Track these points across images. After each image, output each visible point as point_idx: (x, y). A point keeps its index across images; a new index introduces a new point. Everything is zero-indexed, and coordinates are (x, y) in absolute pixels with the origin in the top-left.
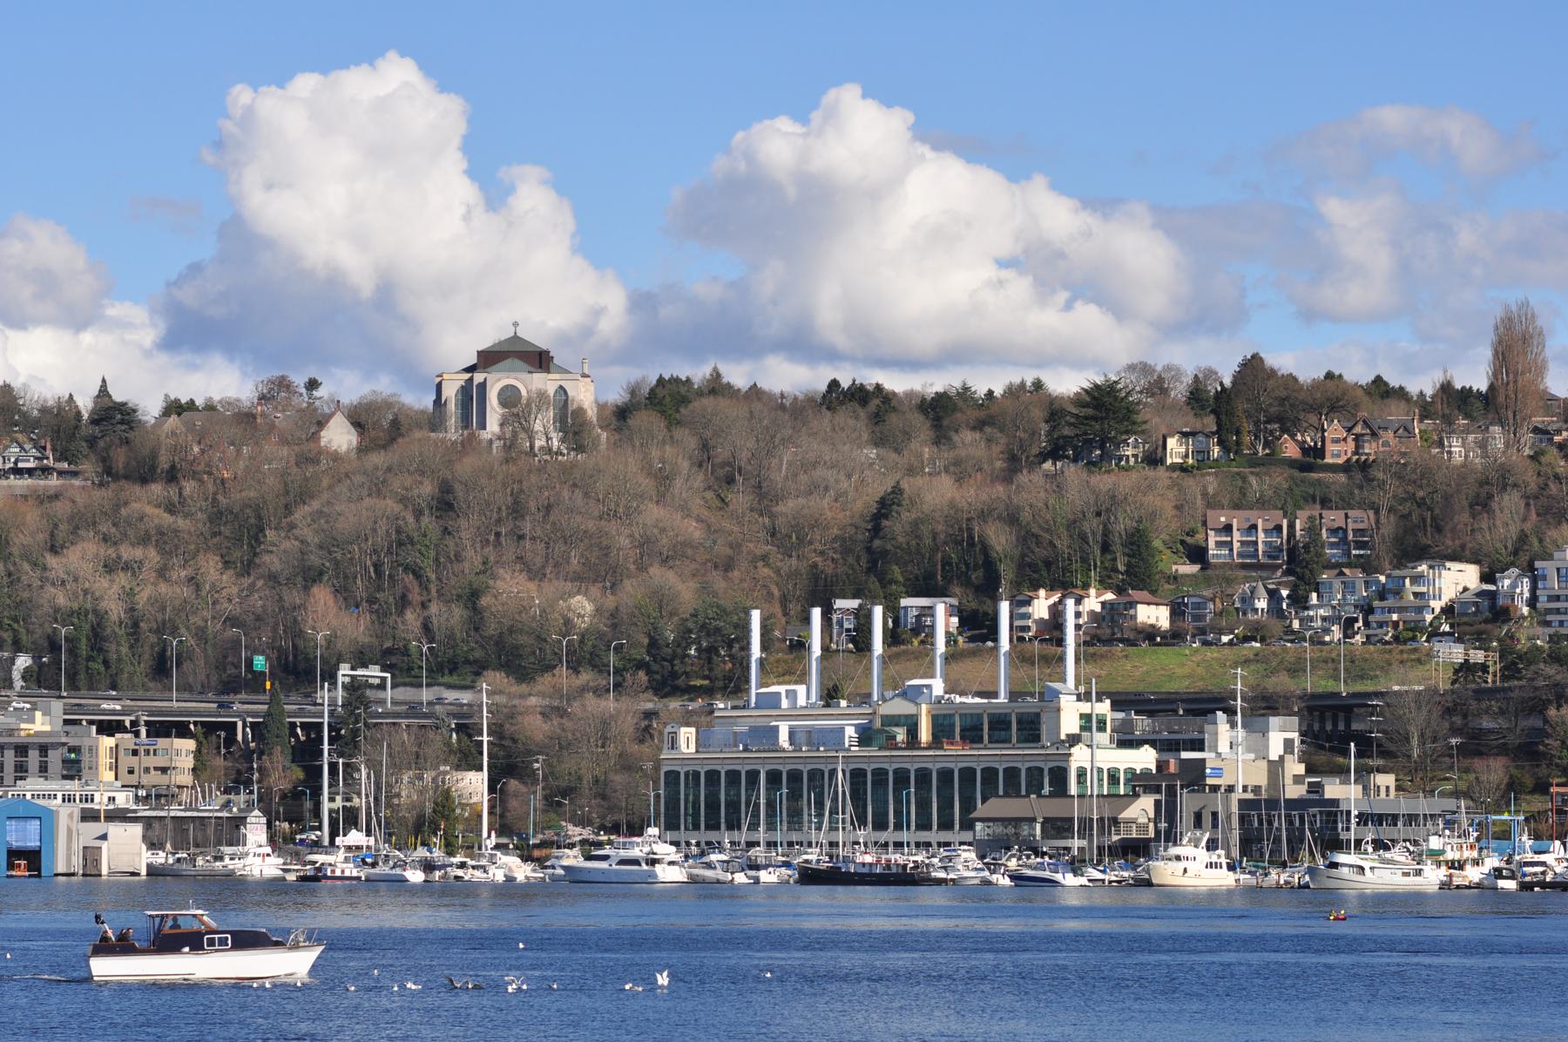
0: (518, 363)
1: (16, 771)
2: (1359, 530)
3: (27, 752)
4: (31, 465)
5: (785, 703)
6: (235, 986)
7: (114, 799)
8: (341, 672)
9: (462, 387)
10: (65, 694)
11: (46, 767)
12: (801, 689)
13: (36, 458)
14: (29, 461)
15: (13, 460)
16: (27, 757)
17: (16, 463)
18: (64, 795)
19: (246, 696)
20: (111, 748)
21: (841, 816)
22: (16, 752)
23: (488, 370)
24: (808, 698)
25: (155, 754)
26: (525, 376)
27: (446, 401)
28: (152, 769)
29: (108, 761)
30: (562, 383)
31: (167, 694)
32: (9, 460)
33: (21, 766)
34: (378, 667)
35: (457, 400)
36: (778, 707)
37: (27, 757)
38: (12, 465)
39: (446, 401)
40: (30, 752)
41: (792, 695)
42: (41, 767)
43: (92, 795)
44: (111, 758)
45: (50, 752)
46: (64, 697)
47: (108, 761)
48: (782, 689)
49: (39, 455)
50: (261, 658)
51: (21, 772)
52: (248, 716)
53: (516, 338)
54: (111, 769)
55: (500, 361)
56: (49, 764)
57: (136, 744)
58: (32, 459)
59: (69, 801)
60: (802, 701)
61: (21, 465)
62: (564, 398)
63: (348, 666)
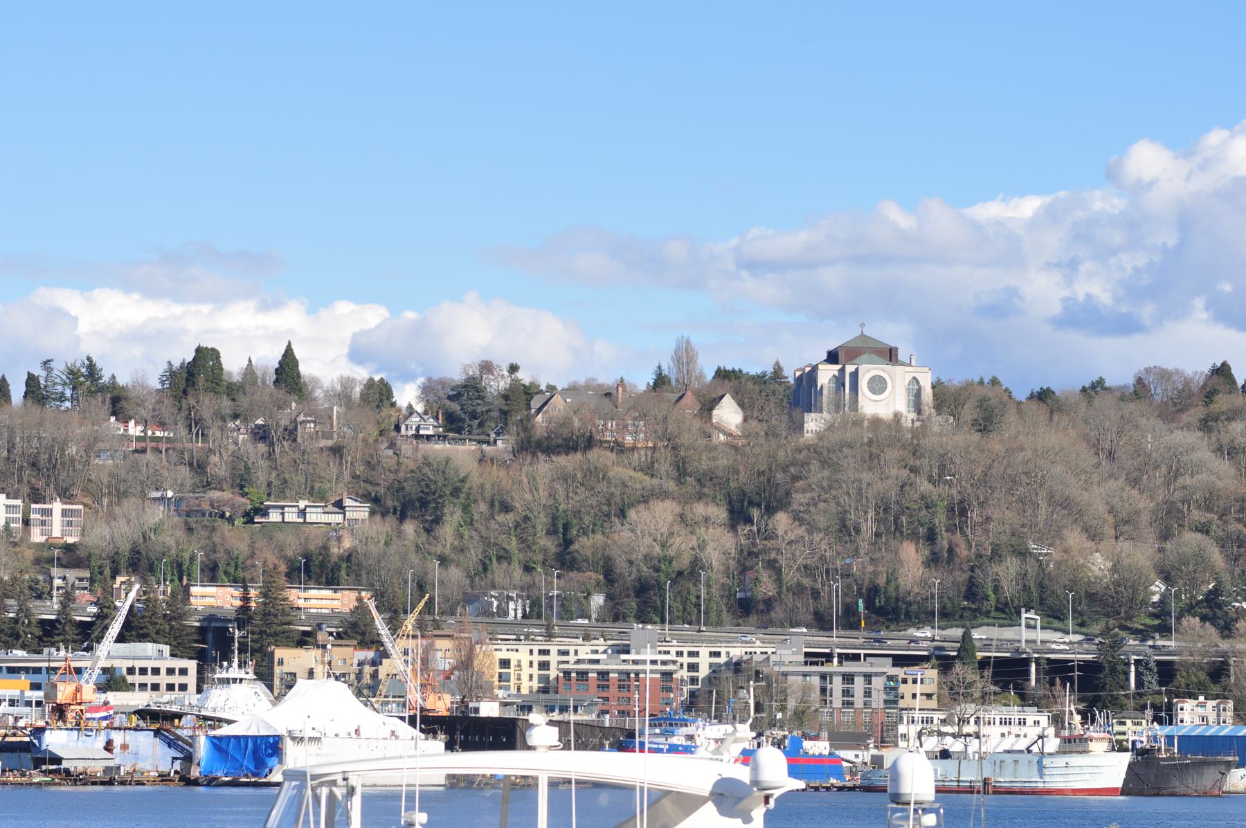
0: (874, 357)
1: (843, 696)
2: (10, 506)
3: (853, 680)
4: (430, 432)
7: (1038, 722)
9: (834, 376)
10: (704, 629)
11: (870, 692)
13: (434, 427)
14: (428, 429)
15: (414, 428)
16: (853, 684)
17: (418, 429)
18: (1001, 719)
19: (842, 633)
21: (637, 740)
22: (843, 679)
25: (922, 683)
27: (822, 387)
28: (137, 686)
30: (916, 375)
31: (829, 633)
32: (411, 428)
33: (848, 691)
37: (853, 684)
38: (414, 432)
39: (822, 387)
42: (865, 692)
43: (1024, 719)
45: (873, 679)
46: (703, 631)
51: (848, 696)
52: (1134, 654)
53: (863, 337)
57: (905, 674)
58: (431, 427)
59: (1005, 723)
61: (422, 432)
62: (916, 387)
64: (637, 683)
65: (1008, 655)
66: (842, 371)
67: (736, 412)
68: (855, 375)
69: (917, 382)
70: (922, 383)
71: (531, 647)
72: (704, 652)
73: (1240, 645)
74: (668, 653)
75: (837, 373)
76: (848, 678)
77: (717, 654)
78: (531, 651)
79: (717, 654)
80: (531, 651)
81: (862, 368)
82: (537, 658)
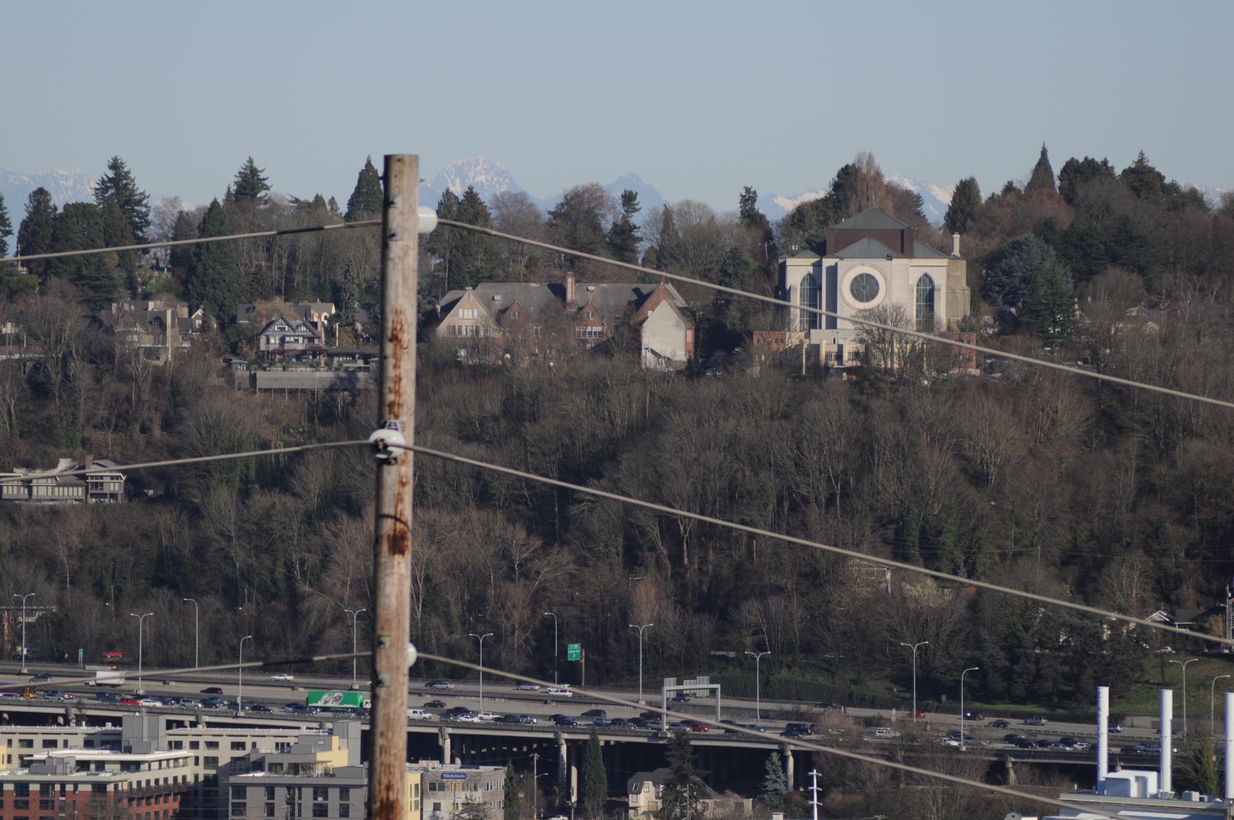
0: (876, 245)
5: (1134, 791)
6: (421, 358)
8: (666, 688)
12: (1152, 776)
20: (417, 786)
23: (840, 253)
24: (1159, 786)
26: (883, 263)
29: (414, 799)
30: (930, 271)
34: (706, 678)
35: (802, 290)
36: (1126, 794)
40: (330, 790)
41: (1143, 782)
44: (416, 795)
47: (414, 799)
48: (1130, 775)
49: (310, 334)
50: (576, 646)
54: (416, 808)
55: (854, 242)
56: (351, 807)
58: (301, 339)
60: (1152, 789)
63: (673, 680)
64: (64, 798)
65: (645, 740)
66: (818, 266)
67: (678, 325)
68: (833, 271)
69: (931, 281)
70: (936, 282)
71: (10, 737)
72: (225, 743)
73: (231, 817)
74: (308, 728)
75: (811, 269)
76: (270, 790)
77: (241, 746)
78: (10, 742)
79: (241, 746)
80: (10, 742)
81: (843, 265)
82: (17, 750)
